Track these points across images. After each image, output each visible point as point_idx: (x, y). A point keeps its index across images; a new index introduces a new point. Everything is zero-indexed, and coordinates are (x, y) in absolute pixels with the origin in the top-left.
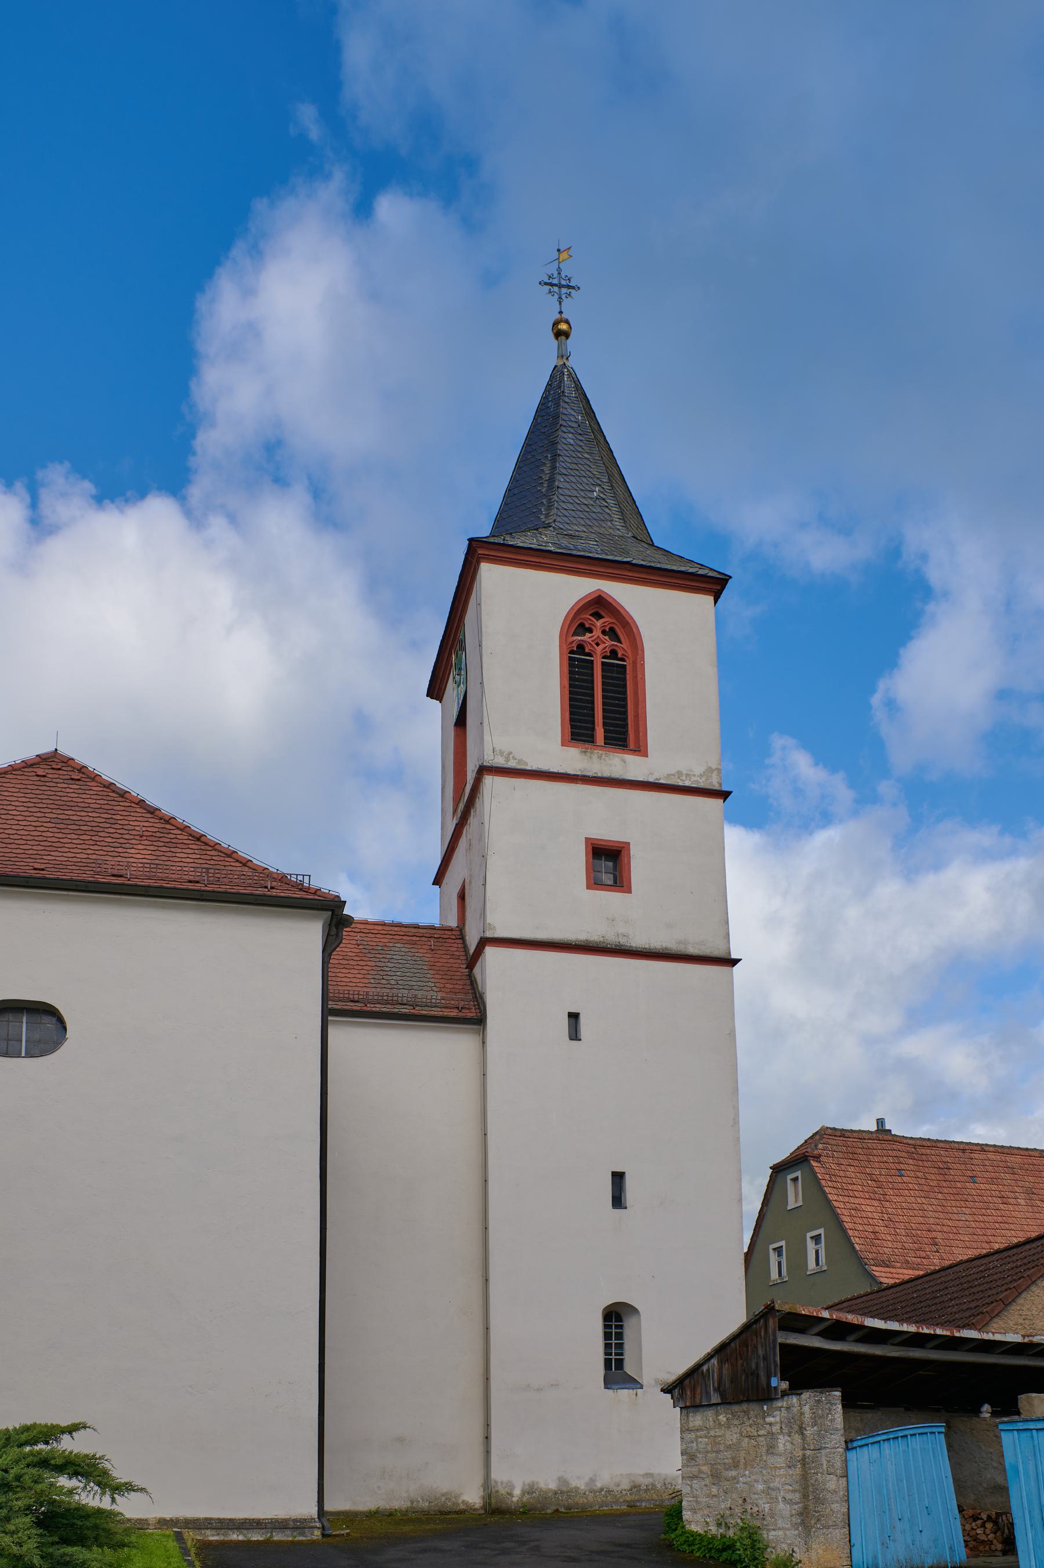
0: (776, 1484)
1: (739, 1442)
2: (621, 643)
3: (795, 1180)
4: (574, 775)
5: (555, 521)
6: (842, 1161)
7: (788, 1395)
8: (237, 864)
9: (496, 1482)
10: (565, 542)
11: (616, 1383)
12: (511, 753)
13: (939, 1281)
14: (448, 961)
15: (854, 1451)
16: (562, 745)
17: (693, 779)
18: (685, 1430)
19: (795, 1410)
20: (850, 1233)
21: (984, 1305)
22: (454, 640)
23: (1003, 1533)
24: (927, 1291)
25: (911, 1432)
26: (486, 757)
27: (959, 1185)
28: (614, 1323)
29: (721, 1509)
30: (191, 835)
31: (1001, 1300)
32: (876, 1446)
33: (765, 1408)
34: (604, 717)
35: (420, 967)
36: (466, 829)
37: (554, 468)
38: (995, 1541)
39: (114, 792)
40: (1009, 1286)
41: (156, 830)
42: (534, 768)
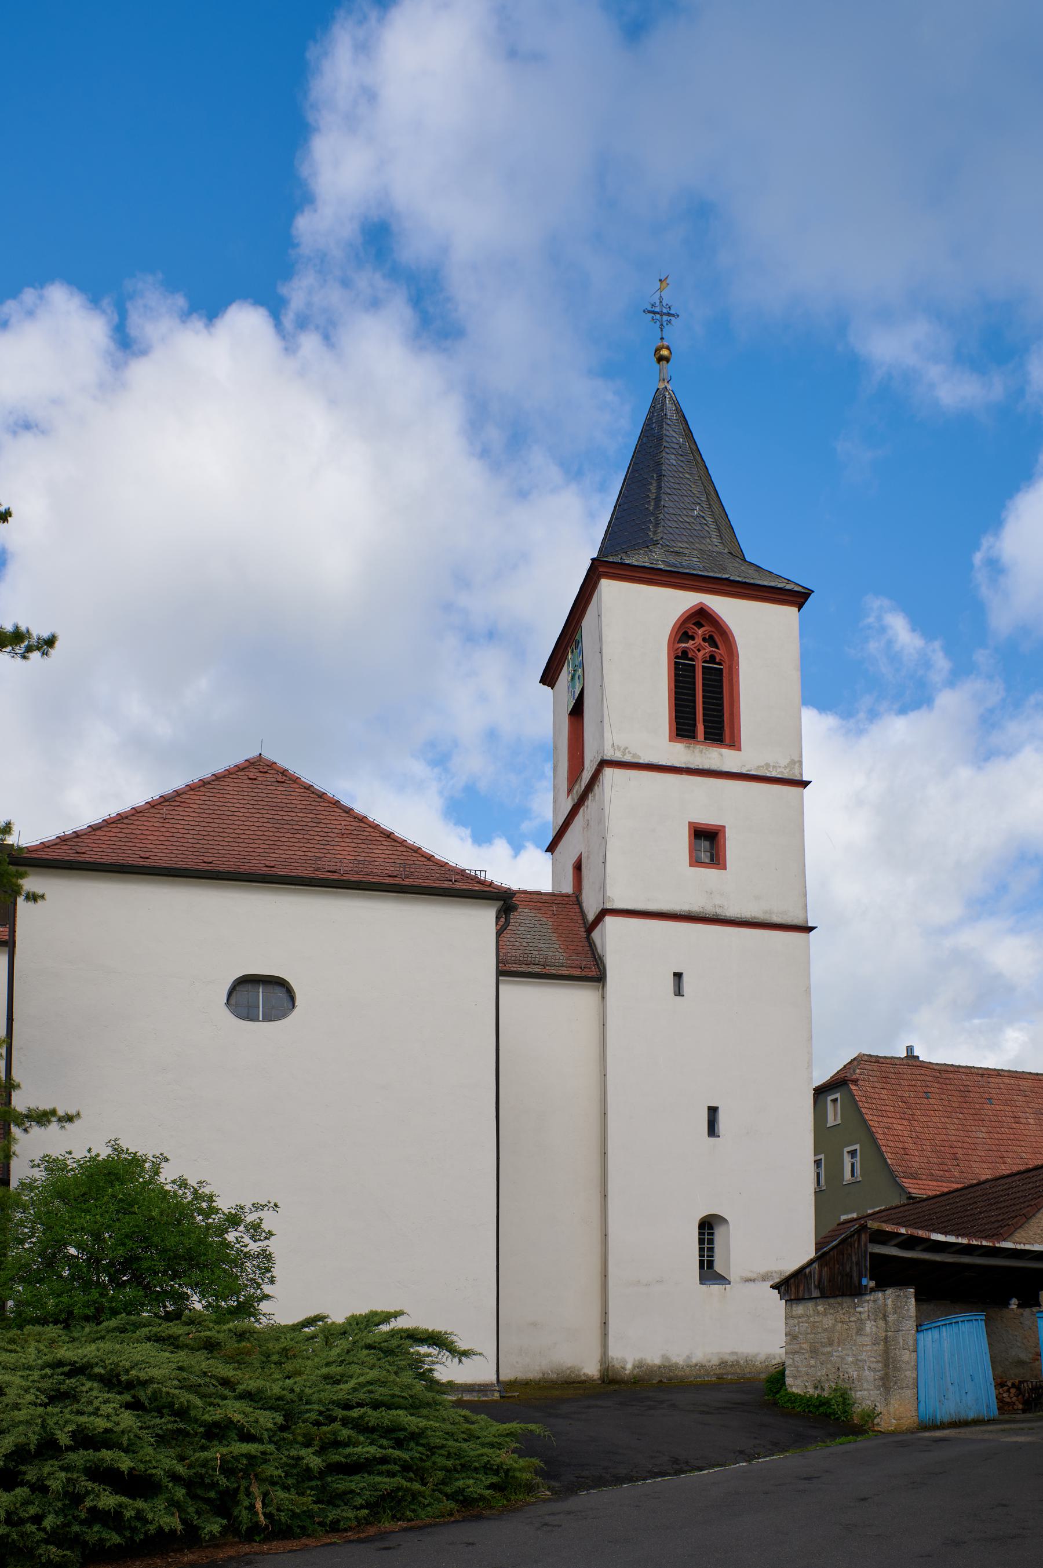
0: (864, 1356)
1: (834, 1326)
2: (718, 648)
3: (835, 1101)
4: (680, 767)
5: (662, 538)
6: (877, 1085)
7: (875, 1291)
8: (423, 859)
9: (613, 1359)
10: (672, 559)
11: (709, 1280)
12: (627, 748)
13: (969, 1196)
14: (569, 924)
15: (922, 1333)
16: (670, 741)
17: (779, 770)
18: (788, 1317)
19: (880, 1302)
20: (883, 1149)
21: (1009, 1218)
22: (570, 639)
23: (1024, 1396)
24: (959, 1204)
25: (961, 1319)
26: (605, 752)
27: (977, 1106)
28: (706, 1231)
29: (818, 1376)
30: (382, 833)
31: (1023, 1214)
32: (937, 1330)
33: (856, 1300)
34: (704, 715)
35: (545, 930)
36: (584, 810)
37: (659, 487)
38: (1017, 1402)
39: (313, 793)
40: (1030, 1203)
41: (353, 828)
42: (646, 762)
